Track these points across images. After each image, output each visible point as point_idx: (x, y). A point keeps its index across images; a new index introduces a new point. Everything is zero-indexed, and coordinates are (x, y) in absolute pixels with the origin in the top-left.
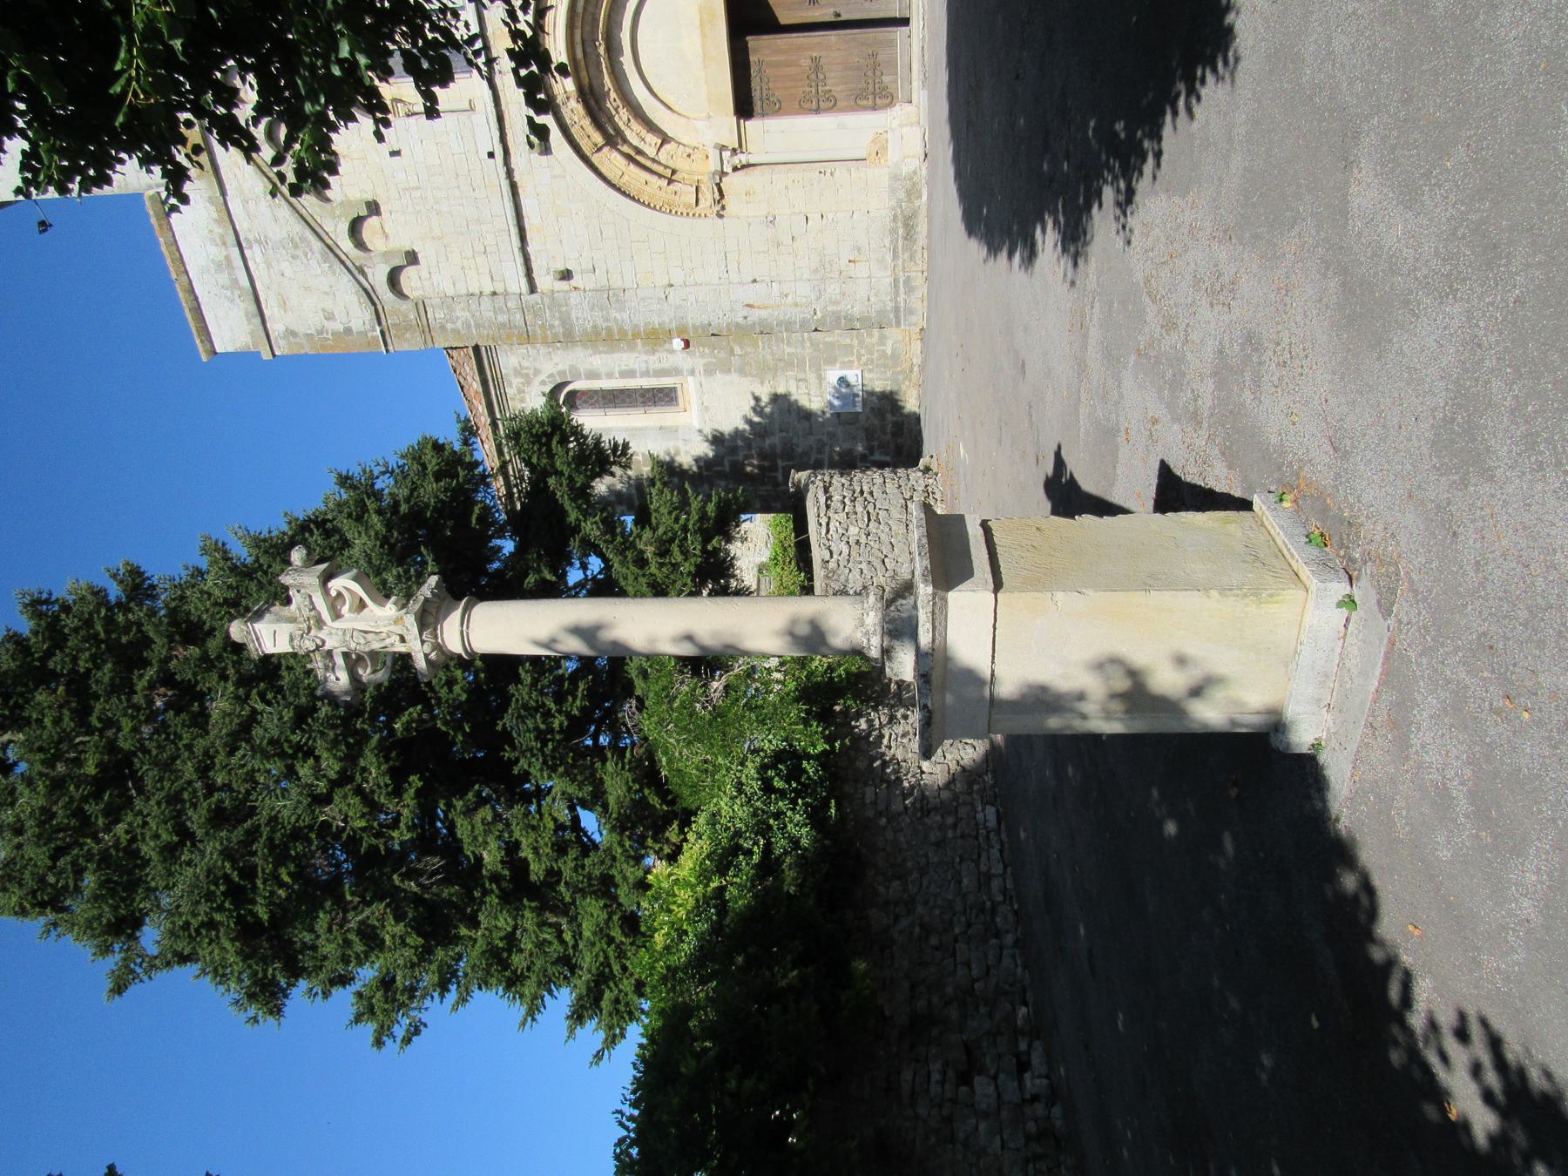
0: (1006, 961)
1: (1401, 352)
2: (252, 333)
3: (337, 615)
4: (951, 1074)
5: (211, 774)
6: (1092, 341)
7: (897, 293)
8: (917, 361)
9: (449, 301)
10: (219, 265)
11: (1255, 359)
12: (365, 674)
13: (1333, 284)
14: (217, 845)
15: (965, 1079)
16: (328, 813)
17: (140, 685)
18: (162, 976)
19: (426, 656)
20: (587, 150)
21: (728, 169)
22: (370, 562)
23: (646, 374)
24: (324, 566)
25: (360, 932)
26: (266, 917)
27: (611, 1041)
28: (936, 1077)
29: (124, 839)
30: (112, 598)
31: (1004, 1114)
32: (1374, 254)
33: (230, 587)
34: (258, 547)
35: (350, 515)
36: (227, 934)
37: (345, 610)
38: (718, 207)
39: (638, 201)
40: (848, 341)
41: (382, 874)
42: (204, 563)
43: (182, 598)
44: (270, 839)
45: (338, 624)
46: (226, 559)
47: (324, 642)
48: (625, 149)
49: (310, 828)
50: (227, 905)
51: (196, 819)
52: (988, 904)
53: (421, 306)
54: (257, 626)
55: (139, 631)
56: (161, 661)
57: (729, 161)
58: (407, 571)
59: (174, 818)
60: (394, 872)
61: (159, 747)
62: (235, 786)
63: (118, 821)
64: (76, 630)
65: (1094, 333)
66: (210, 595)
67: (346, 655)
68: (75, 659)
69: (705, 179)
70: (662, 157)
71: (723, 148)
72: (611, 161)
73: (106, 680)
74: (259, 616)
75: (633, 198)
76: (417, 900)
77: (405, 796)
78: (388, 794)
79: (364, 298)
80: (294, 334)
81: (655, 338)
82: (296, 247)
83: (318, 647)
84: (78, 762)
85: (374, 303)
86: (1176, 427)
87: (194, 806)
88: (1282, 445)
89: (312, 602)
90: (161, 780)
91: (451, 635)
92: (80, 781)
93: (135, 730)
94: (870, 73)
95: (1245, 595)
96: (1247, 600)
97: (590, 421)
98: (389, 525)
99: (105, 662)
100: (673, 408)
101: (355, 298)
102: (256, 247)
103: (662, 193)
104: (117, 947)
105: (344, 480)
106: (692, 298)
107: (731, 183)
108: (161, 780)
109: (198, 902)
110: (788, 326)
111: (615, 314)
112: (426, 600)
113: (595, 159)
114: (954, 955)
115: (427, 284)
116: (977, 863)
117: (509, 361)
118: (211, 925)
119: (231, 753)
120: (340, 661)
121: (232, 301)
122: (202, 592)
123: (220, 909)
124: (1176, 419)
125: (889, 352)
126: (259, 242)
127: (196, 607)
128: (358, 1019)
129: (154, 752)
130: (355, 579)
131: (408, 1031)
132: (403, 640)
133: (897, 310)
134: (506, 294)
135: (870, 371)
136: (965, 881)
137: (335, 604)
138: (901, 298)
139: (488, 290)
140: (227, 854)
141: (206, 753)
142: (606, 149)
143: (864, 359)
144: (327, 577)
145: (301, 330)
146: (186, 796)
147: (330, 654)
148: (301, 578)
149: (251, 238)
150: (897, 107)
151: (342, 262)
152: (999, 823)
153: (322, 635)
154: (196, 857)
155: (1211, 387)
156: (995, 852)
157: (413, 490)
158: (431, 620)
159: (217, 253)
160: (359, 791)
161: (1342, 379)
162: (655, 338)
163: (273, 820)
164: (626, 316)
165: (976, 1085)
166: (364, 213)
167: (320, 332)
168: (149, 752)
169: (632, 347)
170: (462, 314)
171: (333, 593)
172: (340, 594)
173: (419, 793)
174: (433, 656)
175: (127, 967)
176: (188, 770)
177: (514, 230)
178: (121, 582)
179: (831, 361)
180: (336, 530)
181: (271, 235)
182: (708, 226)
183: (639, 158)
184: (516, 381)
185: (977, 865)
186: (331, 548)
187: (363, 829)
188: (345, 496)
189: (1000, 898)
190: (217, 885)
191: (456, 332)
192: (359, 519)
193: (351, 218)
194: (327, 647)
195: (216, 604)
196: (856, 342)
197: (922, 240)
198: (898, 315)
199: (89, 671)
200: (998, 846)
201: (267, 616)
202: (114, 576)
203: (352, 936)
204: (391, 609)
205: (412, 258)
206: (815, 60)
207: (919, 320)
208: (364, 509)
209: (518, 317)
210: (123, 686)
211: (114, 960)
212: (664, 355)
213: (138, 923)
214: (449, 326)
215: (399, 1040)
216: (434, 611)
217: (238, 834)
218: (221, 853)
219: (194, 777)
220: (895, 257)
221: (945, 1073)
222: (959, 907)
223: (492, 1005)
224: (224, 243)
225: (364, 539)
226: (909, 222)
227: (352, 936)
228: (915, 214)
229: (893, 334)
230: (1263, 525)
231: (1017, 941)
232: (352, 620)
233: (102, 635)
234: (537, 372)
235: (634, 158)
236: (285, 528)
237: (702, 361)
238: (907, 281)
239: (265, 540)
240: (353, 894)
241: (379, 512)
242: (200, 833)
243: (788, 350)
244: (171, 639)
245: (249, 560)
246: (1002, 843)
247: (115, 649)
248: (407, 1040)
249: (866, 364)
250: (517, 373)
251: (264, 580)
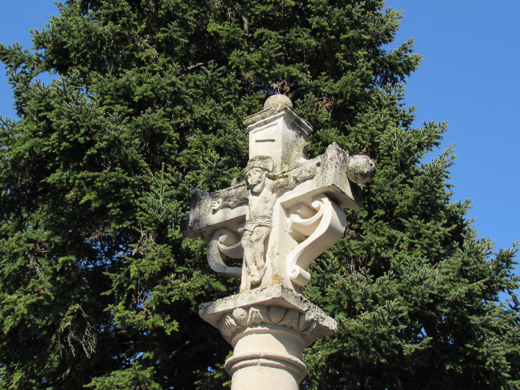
5: (199, 131)
12: (219, 245)
14: (125, 135)
16: (148, 243)
17: (294, 70)
18: (9, 91)
19: (230, 312)
22: (413, 283)
24: (349, 192)
25: (23, 268)
26: (49, 180)
29: (142, 56)
30: (383, 47)
33: (390, 148)
34: (432, 174)
35: (466, 264)
36: (37, 145)
37: (295, 218)
41: (82, 293)
42: (417, 125)
43: (380, 106)
44: (126, 184)
45: (278, 210)
46: (420, 146)
49: (135, 222)
50: (64, 144)
51: (154, 117)
54: (281, 122)
55: (347, 68)
56: (317, 87)
58: (402, 319)
59: (158, 98)
60: (85, 306)
61: (229, 84)
62: (185, 151)
63: (160, 50)
64: (349, 15)
66: (382, 130)
67: (241, 220)
68: (321, 14)
73: (300, 40)
74: (294, 124)
76: (52, 328)
77: (157, 316)
78: (160, 299)
83: (250, 187)
84: (222, 18)
87: (169, 116)
89: (304, 180)
90: (197, 86)
91: (254, 344)
92: (202, 20)
93: (248, 64)
98: (455, 304)
99: (318, 39)
104: (42, 51)
105: (505, 260)
108: (197, 86)
109: (70, 117)
112: (301, 314)
118: (48, 131)
119: (219, 150)
120: (233, 214)
122: (386, 123)
123: (62, 138)
127: (369, 118)
129: (223, 80)
130: (331, 229)
132: (255, 285)
137: (302, 206)
140: (115, 144)
141: (219, 126)
144: (335, 197)
146: (179, 108)
147: (245, 202)
148: (335, 167)
153: (266, 193)
154: (115, 116)
157: (497, 331)
158: (275, 319)
160: (166, 270)
163: (146, 187)
168: (225, 75)
171: (315, 204)
172: (315, 211)
173: (161, 330)
174: (230, 321)
175: (23, 61)
176: (202, 110)
178: (399, 55)
180: (451, 252)
186: (431, 245)
187: (128, 274)
188: (488, 260)
190: (86, 134)
192: (462, 273)
194: (251, 197)
195: (373, 135)
199: (309, 26)
201: (292, 134)
202: (404, 48)
203: (20, 261)
208: (473, 279)
210: (292, 54)
211: (30, 49)
213: (62, 69)
216: (286, 322)
217: (133, 153)
218: (116, 138)
219: (196, 115)
225: (440, 278)
227: (20, 261)
233: (343, 37)
236: (452, 202)
239: (439, 180)
240: (65, 263)
241: (470, 295)
242: (139, 120)
244: (340, 95)
245: (418, 167)
247: (331, 47)
251: (396, 180)
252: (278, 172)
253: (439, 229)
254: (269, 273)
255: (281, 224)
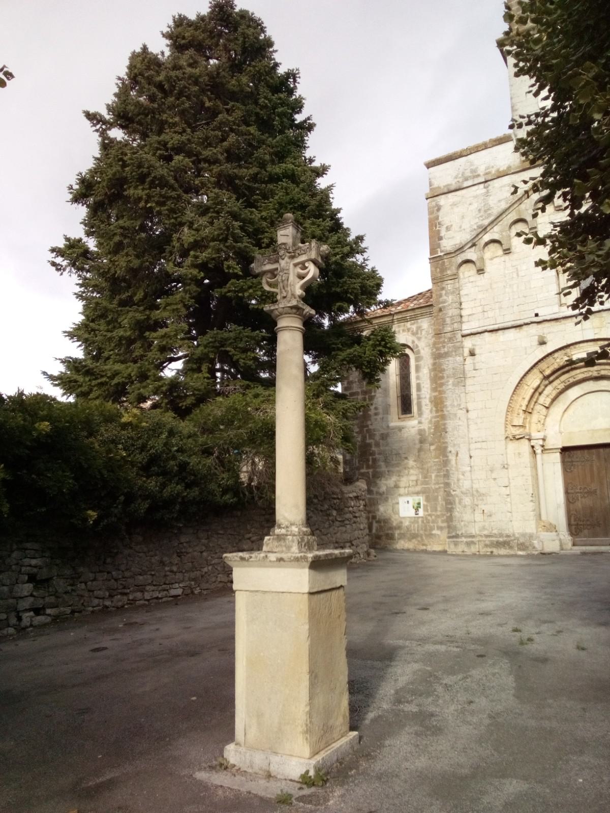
0: (96, 601)
1: (431, 805)
2: (439, 187)
3: (295, 265)
4: (35, 570)
6: (438, 647)
7: (466, 537)
8: (429, 548)
9: (457, 292)
10: (473, 171)
11: (429, 733)
13: (465, 771)
15: (32, 579)
20: (543, 366)
21: (533, 443)
23: (419, 398)
27: (51, 378)
28: (34, 562)
31: (11, 601)
32: (481, 791)
38: (511, 437)
39: (513, 394)
40: (439, 509)
45: (291, 266)
47: (283, 259)
48: (542, 387)
52: (128, 591)
53: (455, 277)
57: (537, 444)
65: (442, 648)
67: (277, 269)
69: (527, 430)
70: (538, 407)
71: (544, 440)
72: (535, 380)
75: (515, 391)
79: (458, 247)
80: (438, 210)
81: (438, 403)
82: (485, 211)
85: (456, 251)
86: (392, 692)
88: (384, 747)
94: (588, 523)
95: (307, 725)
96: (304, 726)
97: (393, 366)
100: (400, 412)
101: (458, 242)
102: (484, 190)
103: (518, 407)
105: (360, 238)
106: (461, 423)
107: (525, 446)
110: (447, 476)
111: (451, 381)
112: (304, 310)
113: (535, 370)
114: (100, 571)
115: (466, 280)
116: (151, 584)
117: (425, 324)
118: (124, 165)
121: (456, 178)
124: (397, 692)
125: (434, 532)
126: (488, 192)
128: (68, 239)
130: (313, 278)
131: (59, 265)
133: (457, 536)
134: (461, 322)
135: (423, 522)
136: (141, 578)
138: (464, 539)
139: (464, 313)
142: (541, 376)
143: (429, 518)
144: (314, 262)
145: (441, 214)
147: (277, 261)
148: (313, 250)
149: (490, 188)
150: (570, 538)
151: (478, 235)
152: (172, 597)
155: (414, 710)
156: (156, 594)
159: (481, 170)
161: (418, 776)
162: (438, 403)
164: (450, 387)
165: (27, 585)
166: (505, 247)
167: (439, 224)
169: (434, 390)
170: (450, 299)
172: (306, 268)
177: (496, 327)
179: (427, 499)
181: (491, 198)
182: (500, 432)
183: (537, 394)
184: (414, 327)
185: (149, 584)
189: (131, 597)
191: (441, 296)
193: (501, 240)
196: (439, 513)
197: (496, 551)
198: (454, 536)
200: (160, 596)
204: (299, 292)
205: (481, 271)
206: (595, 491)
207: (451, 549)
209: (449, 329)
211: (104, 112)
212: (429, 407)
214: (444, 292)
215: (53, 260)
220: (487, 536)
221: (35, 567)
222: (127, 574)
223: (73, 313)
224: (487, 174)
226: (505, 544)
228: (511, 548)
229: (443, 535)
230: (342, 737)
231: (107, 607)
232: (294, 273)
234: (419, 339)
235: (537, 391)
237: (426, 428)
238: (473, 543)
243: (433, 476)
246: (161, 598)
248: (53, 264)
249: (426, 518)
250: (419, 328)
252: (291, 250)
253: (328, 223)
254: (290, 293)
255: (293, 272)
